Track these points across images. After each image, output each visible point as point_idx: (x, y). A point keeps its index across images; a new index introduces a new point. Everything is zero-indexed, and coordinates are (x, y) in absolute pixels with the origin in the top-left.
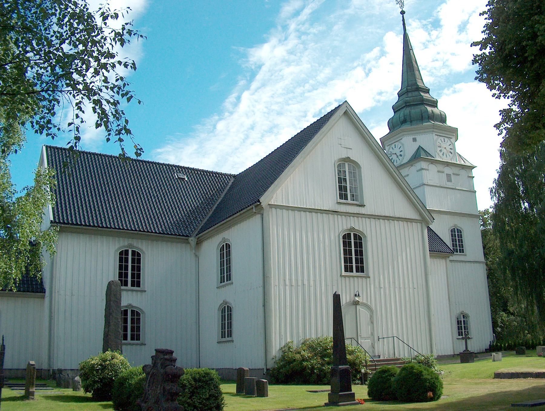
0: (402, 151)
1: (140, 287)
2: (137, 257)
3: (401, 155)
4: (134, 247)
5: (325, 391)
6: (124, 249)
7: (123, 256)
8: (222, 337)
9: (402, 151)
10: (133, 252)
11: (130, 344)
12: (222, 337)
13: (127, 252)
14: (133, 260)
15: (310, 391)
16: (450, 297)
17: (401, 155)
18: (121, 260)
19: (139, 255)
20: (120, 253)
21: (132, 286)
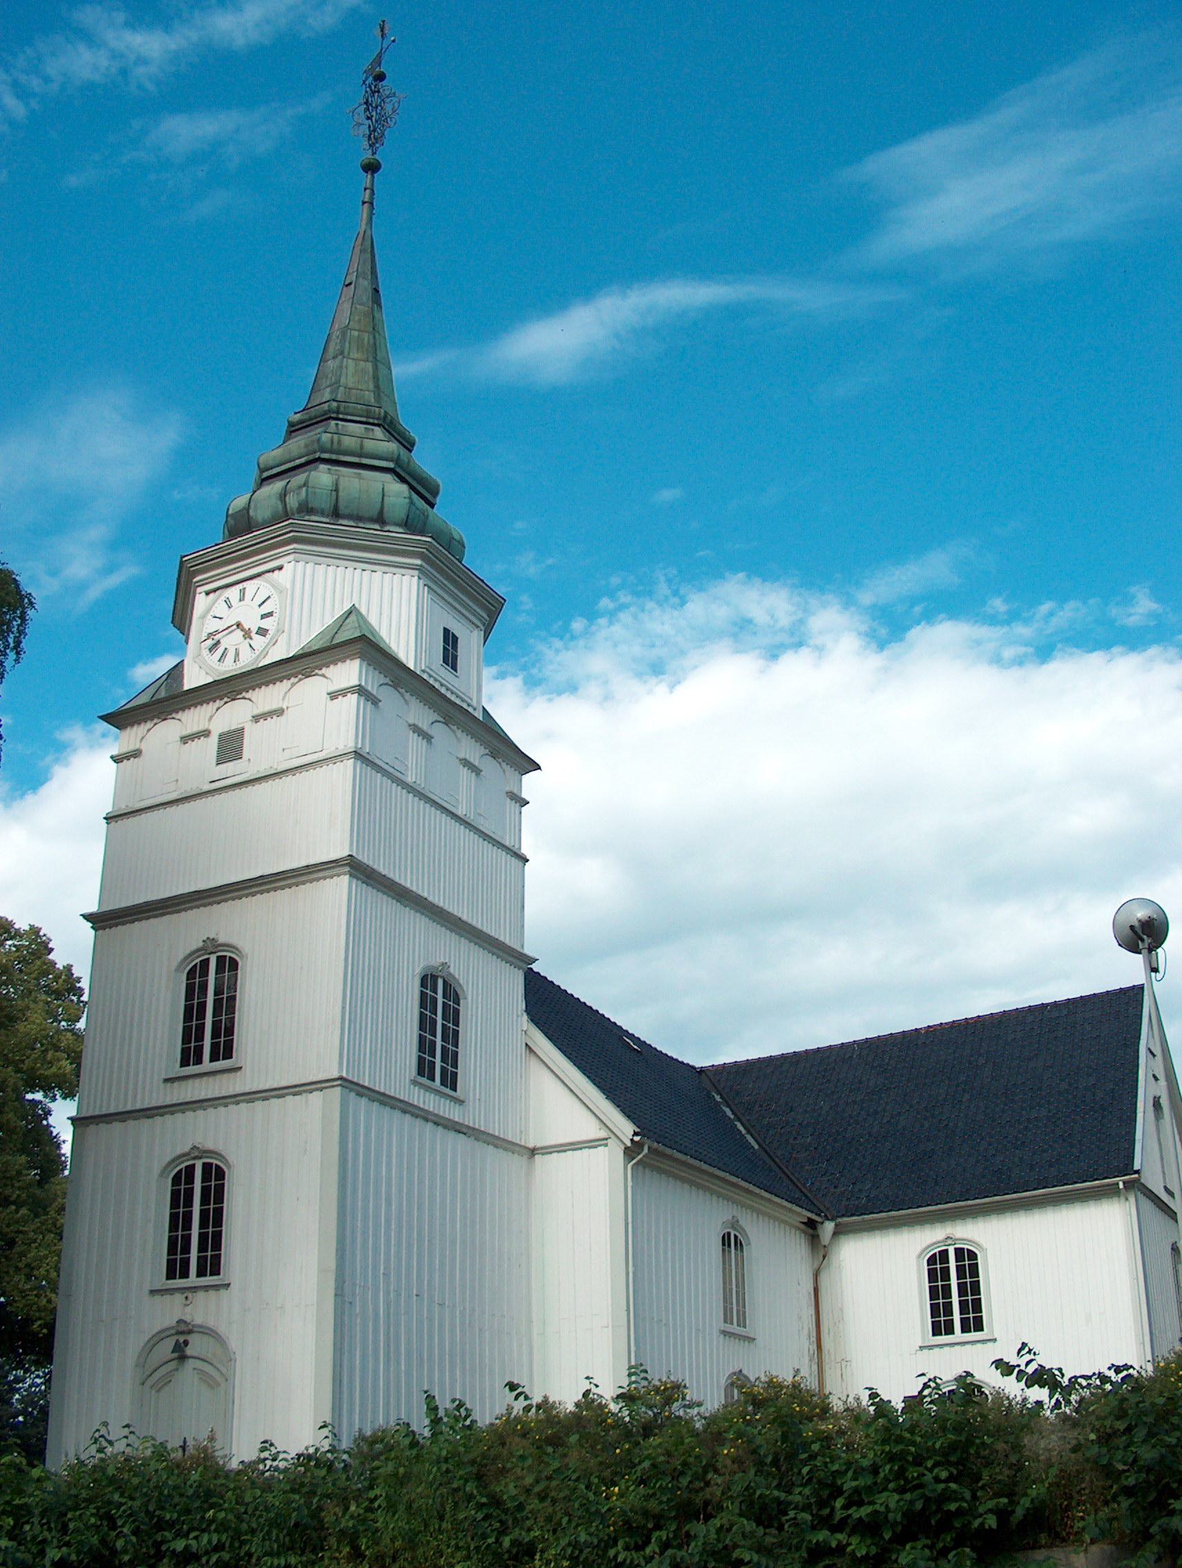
0: (270, 614)
1: (982, 1330)
2: (968, 1261)
3: (262, 632)
4: (955, 1240)
5: (398, 646)
6: (936, 1250)
7: (936, 1265)
8: (168, 1278)
9: (270, 614)
10: (959, 1252)
11: (194, 1289)
12: (168, 1278)
13: (944, 1254)
14: (960, 1270)
15: (212, 1364)
16: (1156, 1332)
17: (262, 632)
18: (932, 1275)
19: (973, 1256)
20: (928, 1261)
21: (963, 1331)
